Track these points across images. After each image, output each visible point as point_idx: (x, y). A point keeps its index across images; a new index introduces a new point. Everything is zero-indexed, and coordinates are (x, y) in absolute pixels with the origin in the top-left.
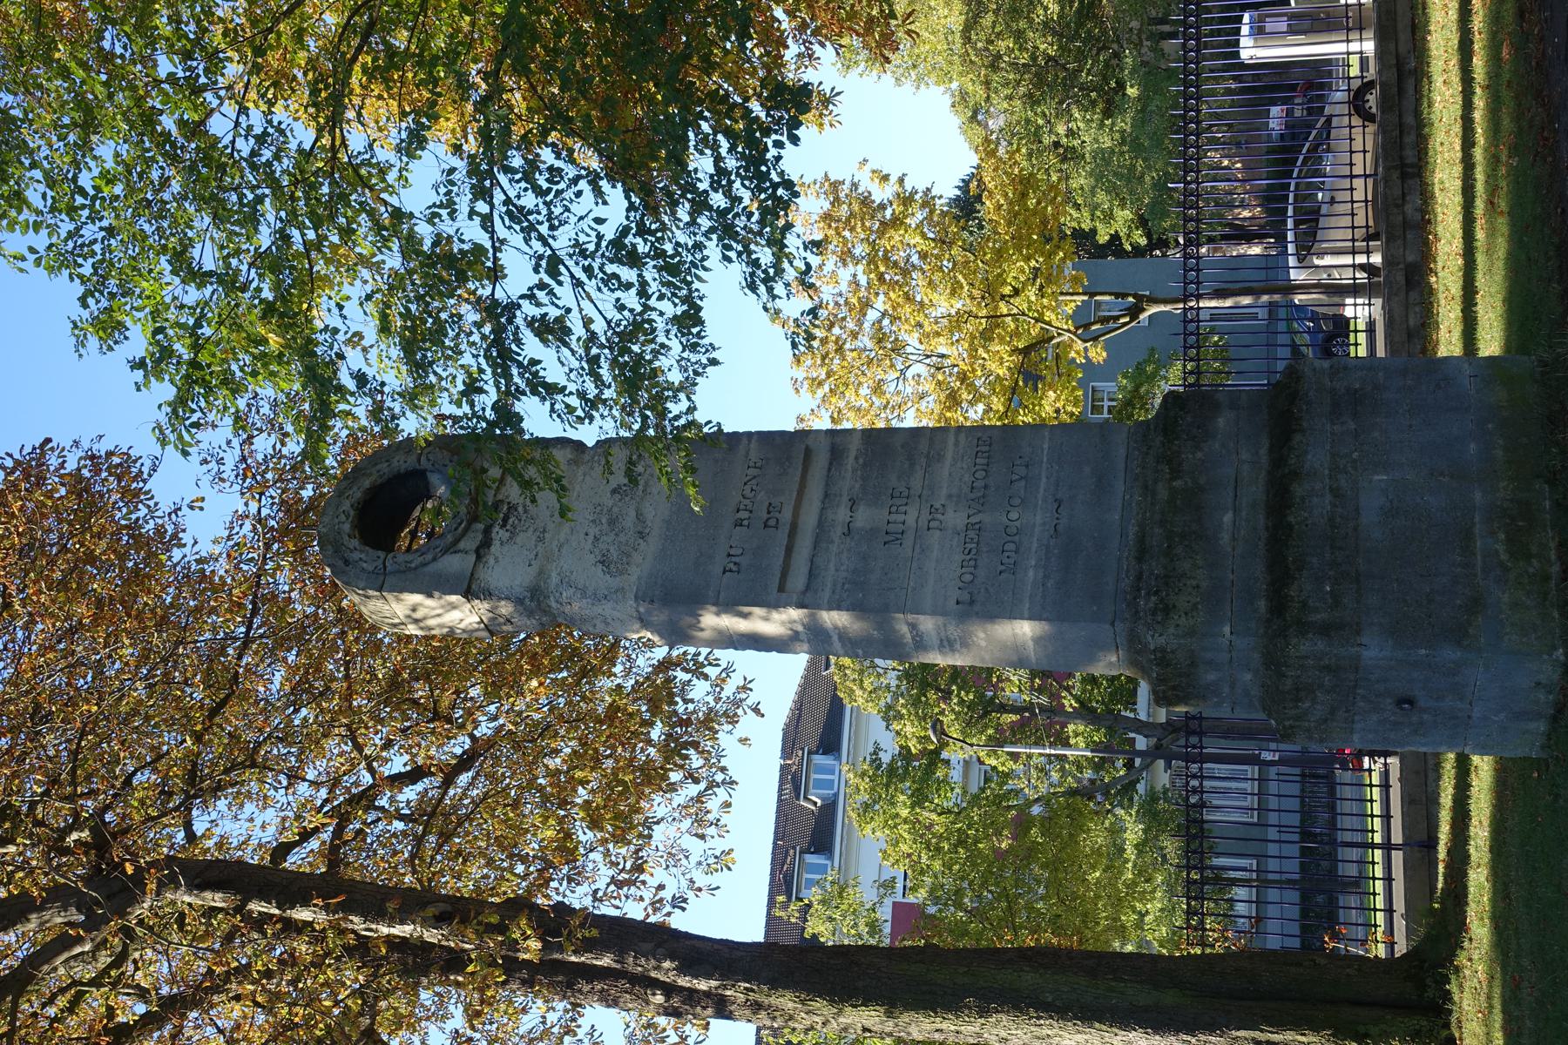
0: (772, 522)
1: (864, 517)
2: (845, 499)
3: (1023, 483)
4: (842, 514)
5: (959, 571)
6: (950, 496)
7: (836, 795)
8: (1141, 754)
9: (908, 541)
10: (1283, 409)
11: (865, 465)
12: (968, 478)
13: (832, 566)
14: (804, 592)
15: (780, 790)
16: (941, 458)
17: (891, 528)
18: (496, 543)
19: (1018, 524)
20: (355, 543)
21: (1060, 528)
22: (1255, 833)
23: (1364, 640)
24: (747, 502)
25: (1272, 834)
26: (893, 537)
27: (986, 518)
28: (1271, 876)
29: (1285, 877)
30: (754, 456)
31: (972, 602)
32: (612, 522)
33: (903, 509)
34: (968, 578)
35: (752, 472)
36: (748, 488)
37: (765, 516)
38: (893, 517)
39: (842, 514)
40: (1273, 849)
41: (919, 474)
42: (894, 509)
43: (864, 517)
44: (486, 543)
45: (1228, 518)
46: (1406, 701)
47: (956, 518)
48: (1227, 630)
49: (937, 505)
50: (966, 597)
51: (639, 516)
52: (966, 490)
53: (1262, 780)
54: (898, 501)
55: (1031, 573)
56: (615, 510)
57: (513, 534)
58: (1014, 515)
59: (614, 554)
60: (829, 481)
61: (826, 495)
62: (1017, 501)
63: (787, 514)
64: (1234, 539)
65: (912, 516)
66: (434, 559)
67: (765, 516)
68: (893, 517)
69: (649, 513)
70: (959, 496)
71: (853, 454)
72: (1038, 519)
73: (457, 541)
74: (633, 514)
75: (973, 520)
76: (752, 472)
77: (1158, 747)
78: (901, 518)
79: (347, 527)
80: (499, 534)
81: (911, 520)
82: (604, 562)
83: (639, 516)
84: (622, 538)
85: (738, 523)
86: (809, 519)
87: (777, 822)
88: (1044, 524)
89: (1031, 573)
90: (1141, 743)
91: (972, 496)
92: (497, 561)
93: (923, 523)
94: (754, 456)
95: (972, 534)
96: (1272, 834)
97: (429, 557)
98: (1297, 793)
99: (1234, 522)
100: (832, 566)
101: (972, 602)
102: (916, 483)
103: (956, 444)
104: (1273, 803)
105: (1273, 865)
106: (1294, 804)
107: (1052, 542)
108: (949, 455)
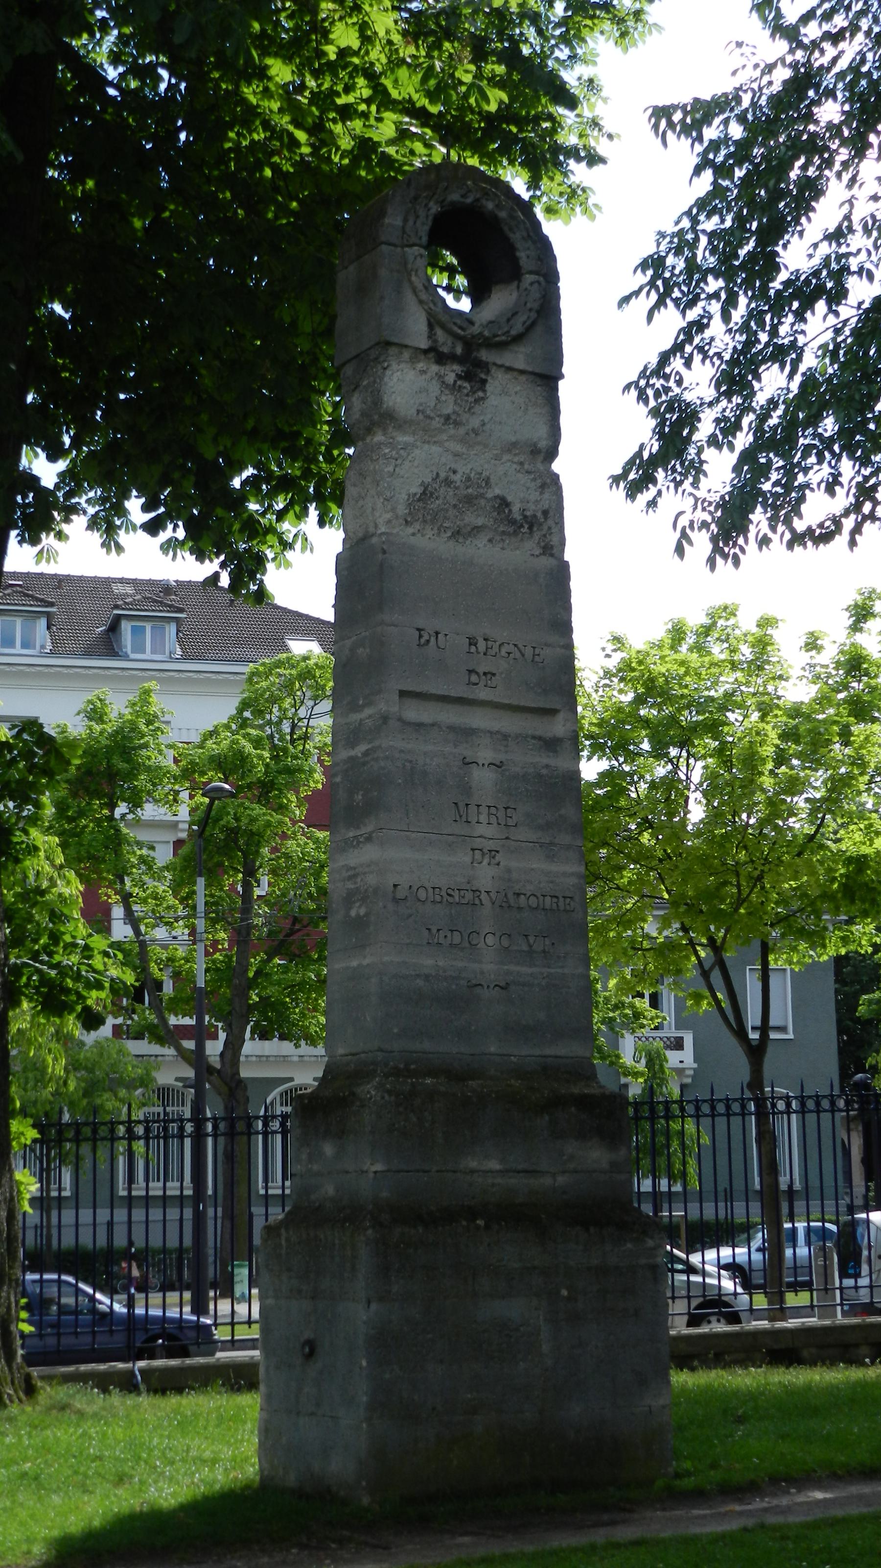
0: (474, 678)
1: (483, 779)
2: (501, 757)
3: (525, 948)
4: (486, 754)
5: (427, 885)
6: (509, 871)
7: (126, 658)
8: (200, 1047)
9: (458, 829)
10: (610, 1216)
11: (540, 776)
12: (529, 889)
13: (430, 748)
14: (400, 719)
15: (122, 581)
16: (551, 858)
17: (473, 809)
18: (442, 370)
19: (482, 945)
20: (435, 208)
21: (478, 990)
22: (103, 1193)
23: (374, 1306)
24: (496, 649)
25: (103, 1215)
26: (462, 810)
27: (487, 910)
28: (54, 1214)
29: (54, 1232)
30: (547, 652)
31: (396, 900)
32: (469, 500)
33: (493, 820)
34: (422, 894)
35: (528, 652)
36: (511, 648)
37: (481, 670)
38: (484, 810)
39: (486, 754)
40: (86, 1215)
41: (532, 836)
42: (493, 810)
43: (483, 779)
44: (441, 358)
45: (494, 1165)
46: (310, 1350)
47: (485, 876)
48: (379, 1167)
49: (498, 857)
50: (401, 893)
51: (476, 530)
52: (517, 888)
53: (181, 1199)
54: (501, 814)
55: (430, 962)
56: (483, 502)
57: (454, 388)
58: (490, 940)
59: (434, 505)
60: (522, 738)
61: (506, 737)
62: (505, 942)
63: (483, 694)
64: (473, 1172)
65: (486, 830)
66: (421, 302)
67: (481, 670)
68: (484, 810)
69: (481, 541)
70: (509, 880)
71: (552, 762)
72: (488, 964)
73: (443, 327)
74: (480, 522)
75: (484, 896)
76: (528, 652)
77: (210, 1070)
78: (483, 818)
79: (454, 197)
80: (451, 373)
81: (481, 830)
82: (426, 494)
83: (476, 530)
84: (452, 513)
85: (472, 642)
86: (479, 719)
87: (81, 579)
88: (482, 973)
89: (430, 962)
90: (214, 1048)
91: (510, 895)
92: (423, 372)
93: (478, 843)
94: (547, 652)
95: (469, 896)
96: (103, 1215)
97: (424, 296)
98: (169, 1245)
99: (487, 1168)
100: (430, 748)
101: (396, 900)
102: (525, 834)
103: (564, 874)
104: (156, 1214)
105: (68, 1216)
106: (156, 1242)
107: (463, 983)
108: (554, 868)
